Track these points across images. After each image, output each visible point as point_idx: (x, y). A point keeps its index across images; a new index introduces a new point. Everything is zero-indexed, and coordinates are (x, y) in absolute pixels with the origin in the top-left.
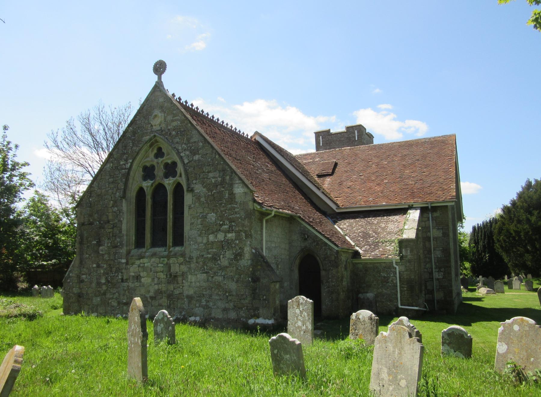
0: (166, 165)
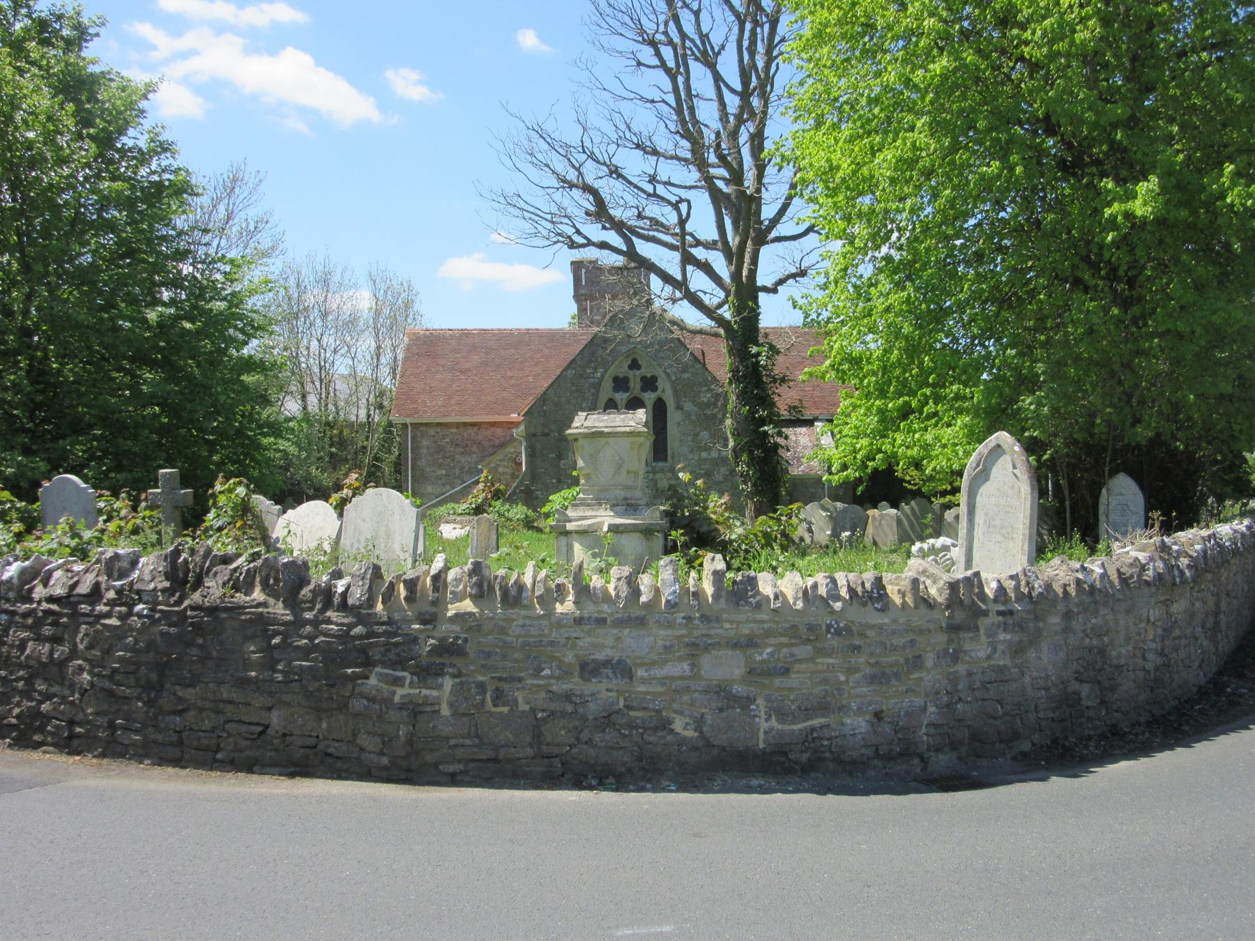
0: (644, 379)
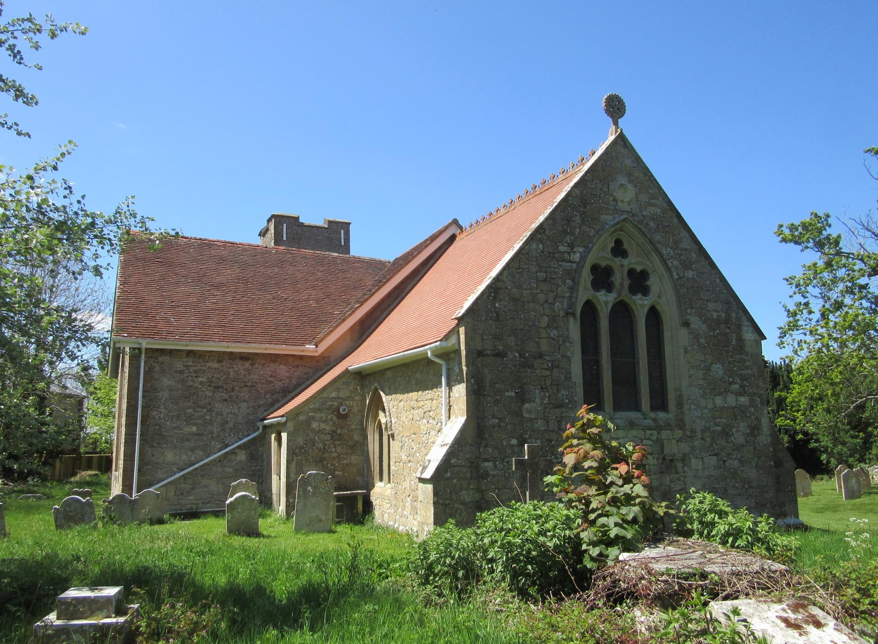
0: (631, 272)
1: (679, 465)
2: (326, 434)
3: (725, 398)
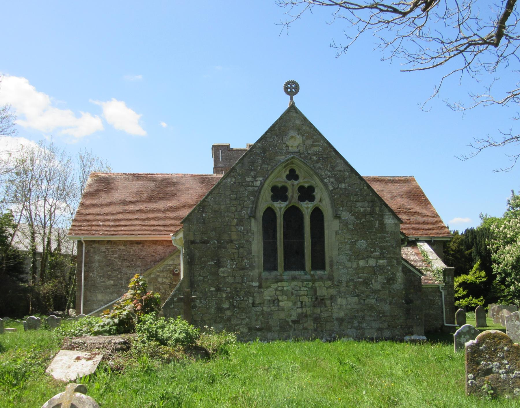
0: (301, 189)
1: (328, 302)
2: (166, 285)
3: (367, 261)
